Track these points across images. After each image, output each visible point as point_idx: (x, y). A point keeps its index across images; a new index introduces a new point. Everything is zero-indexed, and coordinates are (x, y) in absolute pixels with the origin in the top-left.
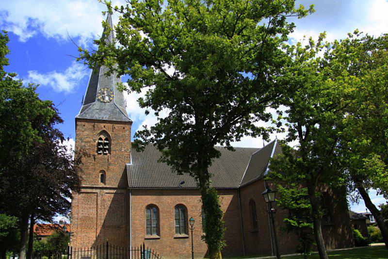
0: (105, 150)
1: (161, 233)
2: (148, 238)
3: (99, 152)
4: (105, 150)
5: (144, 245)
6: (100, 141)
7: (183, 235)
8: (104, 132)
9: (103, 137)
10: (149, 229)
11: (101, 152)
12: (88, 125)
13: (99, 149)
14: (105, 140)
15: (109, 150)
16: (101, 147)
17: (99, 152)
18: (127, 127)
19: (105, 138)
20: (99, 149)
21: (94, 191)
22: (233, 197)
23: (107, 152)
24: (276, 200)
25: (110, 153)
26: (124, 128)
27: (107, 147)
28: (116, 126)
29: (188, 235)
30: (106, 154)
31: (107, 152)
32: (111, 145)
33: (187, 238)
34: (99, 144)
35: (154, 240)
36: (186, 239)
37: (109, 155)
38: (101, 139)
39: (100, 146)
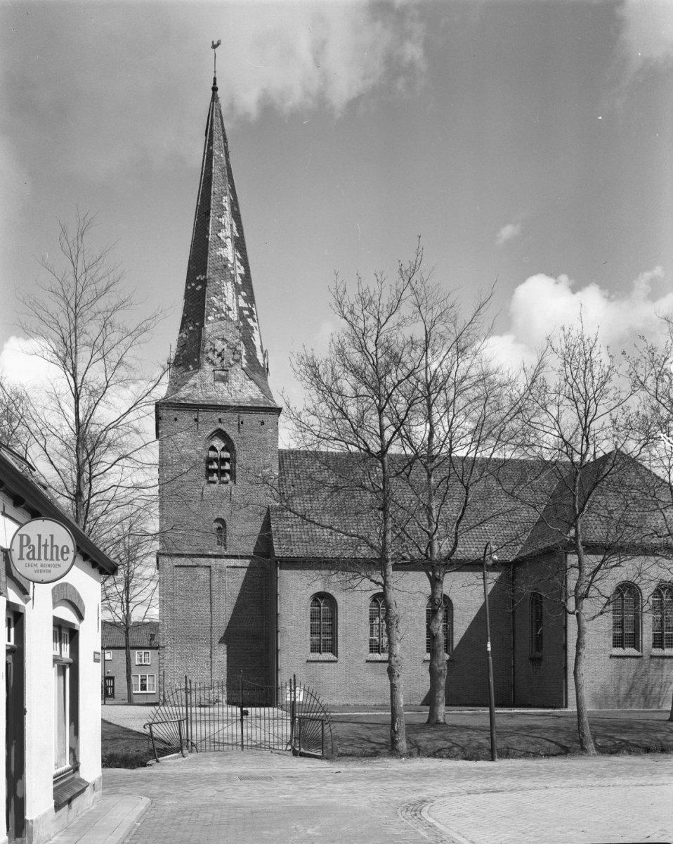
0: (223, 473)
1: (340, 651)
2: (618, 654)
3: (210, 479)
4: (223, 473)
5: (295, 680)
6: (212, 454)
7: (329, 656)
8: (221, 434)
9: (218, 443)
10: (136, 625)
11: (215, 477)
12: (187, 417)
13: (210, 472)
14: (223, 450)
15: (232, 472)
16: (215, 466)
17: (210, 479)
18: (268, 418)
19: (223, 445)
20: (210, 472)
21: (203, 561)
22: (500, 578)
23: (228, 477)
24: (297, 719)
25: (233, 477)
26: (263, 423)
27: (227, 466)
28: (245, 417)
29: (337, 656)
30: (226, 482)
31: (228, 477)
32: (235, 462)
33: (336, 662)
34: (210, 461)
35: (327, 664)
36: (333, 665)
37: (230, 482)
38: (213, 448)
39: (212, 464)
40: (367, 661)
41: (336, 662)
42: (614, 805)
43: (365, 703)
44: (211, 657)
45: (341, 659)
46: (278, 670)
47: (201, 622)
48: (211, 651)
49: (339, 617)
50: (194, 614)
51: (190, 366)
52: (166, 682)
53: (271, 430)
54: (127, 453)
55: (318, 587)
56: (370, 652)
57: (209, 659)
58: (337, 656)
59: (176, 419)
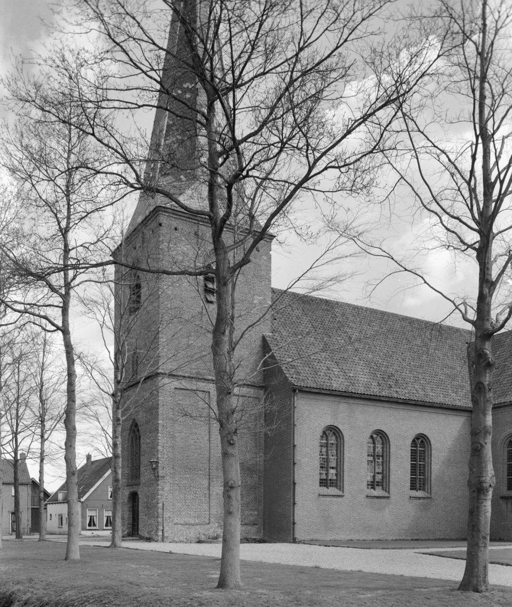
33: (388, 497)
35: (334, 499)
40: (3, 484)
41: (388, 497)
42: (403, 595)
43: (365, 538)
44: (209, 489)
45: (346, 494)
46: (294, 504)
47: (199, 451)
48: (209, 483)
49: (345, 452)
50: (192, 442)
51: (182, 177)
52: (165, 517)
53: (265, 258)
54: (494, 20)
55: (328, 421)
56: (411, 489)
57: (207, 492)
58: (389, 493)
59: (176, 229)
